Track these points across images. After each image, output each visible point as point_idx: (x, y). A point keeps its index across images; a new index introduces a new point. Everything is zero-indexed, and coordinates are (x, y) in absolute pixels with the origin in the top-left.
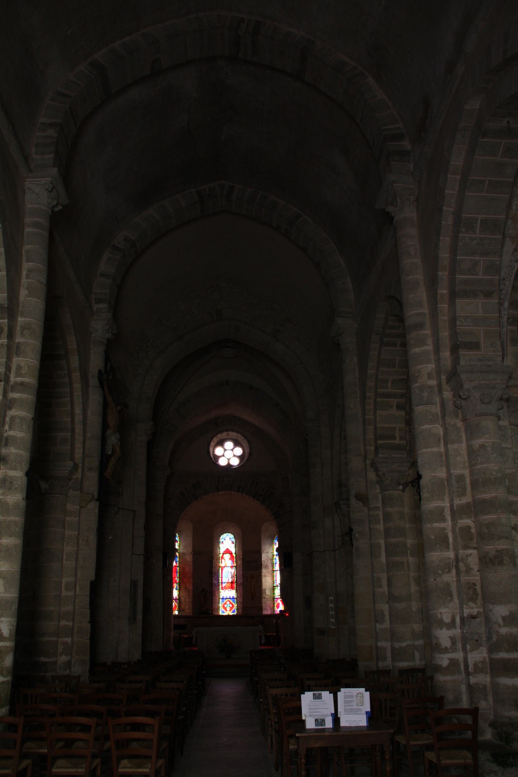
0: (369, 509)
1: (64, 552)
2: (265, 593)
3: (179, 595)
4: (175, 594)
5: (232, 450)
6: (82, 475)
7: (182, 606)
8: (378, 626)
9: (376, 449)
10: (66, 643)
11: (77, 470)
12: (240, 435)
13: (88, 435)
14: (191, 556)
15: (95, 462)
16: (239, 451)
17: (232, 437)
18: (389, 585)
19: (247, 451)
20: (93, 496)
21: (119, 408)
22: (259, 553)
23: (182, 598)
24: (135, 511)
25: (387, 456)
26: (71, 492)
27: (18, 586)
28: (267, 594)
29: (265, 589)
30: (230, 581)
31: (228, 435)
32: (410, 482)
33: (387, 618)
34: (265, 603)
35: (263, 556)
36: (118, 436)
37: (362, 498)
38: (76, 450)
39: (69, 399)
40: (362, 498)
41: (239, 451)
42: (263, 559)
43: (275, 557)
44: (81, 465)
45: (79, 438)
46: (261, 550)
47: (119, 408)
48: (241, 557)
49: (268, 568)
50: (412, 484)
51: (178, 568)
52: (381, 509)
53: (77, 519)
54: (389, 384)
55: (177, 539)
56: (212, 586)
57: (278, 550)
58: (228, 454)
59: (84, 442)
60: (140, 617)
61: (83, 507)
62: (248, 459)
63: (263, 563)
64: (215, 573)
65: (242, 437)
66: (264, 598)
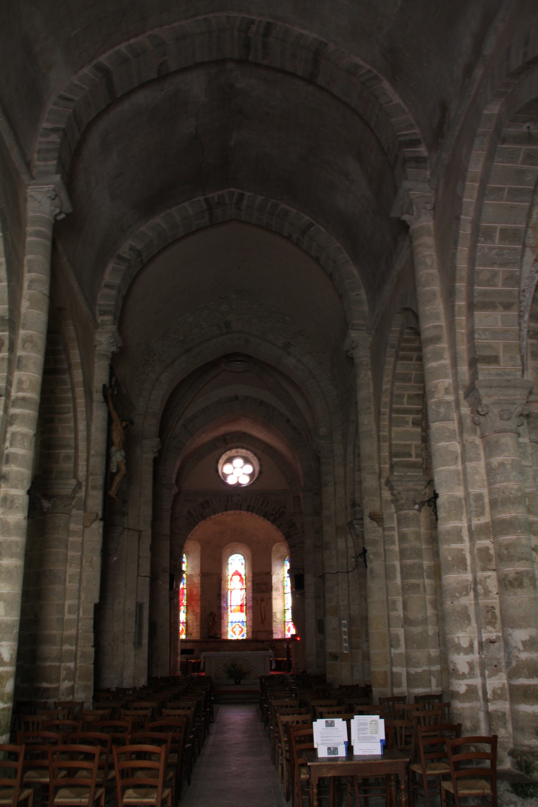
0: (384, 530)
1: (67, 574)
2: (276, 616)
3: (186, 619)
11: (80, 488)
12: (249, 452)
13: (92, 452)
14: (199, 578)
15: (99, 480)
16: (249, 469)
21: (124, 424)
22: (269, 575)
23: (190, 622)
26: (74, 512)
29: (275, 613)
31: (237, 452)
34: (276, 627)
37: (377, 518)
38: (80, 467)
39: (72, 414)
40: (377, 518)
41: (249, 469)
44: (84, 484)
45: (82, 455)
48: (251, 579)
51: (185, 591)
52: (396, 529)
53: (81, 539)
54: (405, 399)
55: (184, 560)
57: (289, 571)
58: (238, 472)
59: (88, 460)
61: (86, 527)
62: (258, 478)
63: (273, 585)
64: (224, 595)
65: (252, 455)
66: (275, 621)
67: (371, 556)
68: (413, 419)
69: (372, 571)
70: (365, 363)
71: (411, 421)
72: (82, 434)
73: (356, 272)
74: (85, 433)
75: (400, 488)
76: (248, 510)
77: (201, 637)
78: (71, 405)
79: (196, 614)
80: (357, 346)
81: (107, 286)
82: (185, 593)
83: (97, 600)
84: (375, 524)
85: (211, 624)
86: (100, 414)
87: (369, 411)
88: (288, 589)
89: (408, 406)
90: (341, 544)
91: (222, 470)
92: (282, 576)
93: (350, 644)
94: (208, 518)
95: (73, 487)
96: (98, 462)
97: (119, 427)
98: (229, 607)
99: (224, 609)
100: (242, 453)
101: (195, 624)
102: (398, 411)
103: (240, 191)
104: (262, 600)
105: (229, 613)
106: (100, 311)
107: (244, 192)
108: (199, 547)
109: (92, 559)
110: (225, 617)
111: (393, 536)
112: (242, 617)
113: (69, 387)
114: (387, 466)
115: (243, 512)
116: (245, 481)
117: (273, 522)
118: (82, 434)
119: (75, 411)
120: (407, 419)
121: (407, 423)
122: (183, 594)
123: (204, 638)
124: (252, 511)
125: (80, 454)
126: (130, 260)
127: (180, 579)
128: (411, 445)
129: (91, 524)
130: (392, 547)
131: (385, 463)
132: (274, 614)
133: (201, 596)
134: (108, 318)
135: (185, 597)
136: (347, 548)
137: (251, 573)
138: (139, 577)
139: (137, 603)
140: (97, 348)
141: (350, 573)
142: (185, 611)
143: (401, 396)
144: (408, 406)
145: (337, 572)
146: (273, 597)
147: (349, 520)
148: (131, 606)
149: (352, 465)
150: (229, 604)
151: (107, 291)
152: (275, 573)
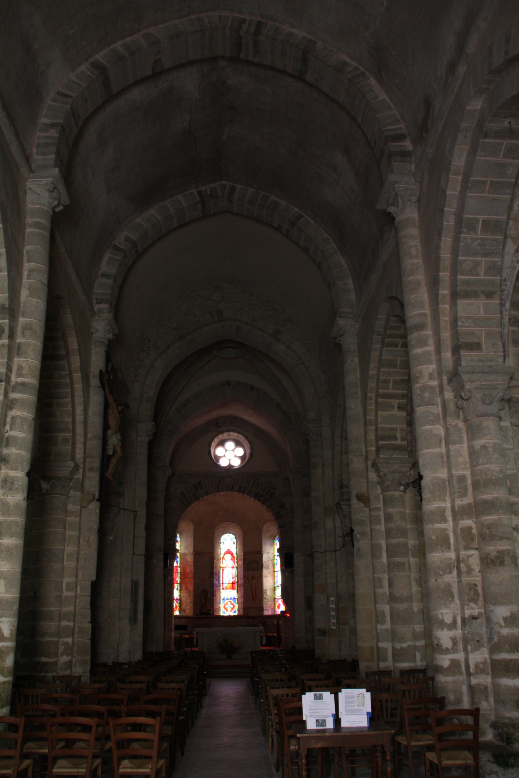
0: (370, 510)
1: (65, 553)
2: (266, 593)
3: (180, 596)
4: (176, 594)
9: (378, 450)
11: (78, 470)
12: (241, 436)
13: (89, 436)
14: (192, 557)
15: (96, 463)
16: (240, 451)
19: (248, 451)
20: (94, 496)
21: (120, 408)
25: (388, 457)
26: (72, 493)
27: (19, 586)
29: (266, 590)
30: (231, 582)
31: (229, 435)
32: (411, 483)
34: (266, 604)
38: (77, 450)
41: (240, 451)
43: (276, 557)
44: (81, 466)
45: (80, 438)
47: (120, 408)
48: (242, 557)
51: (179, 569)
52: (382, 509)
53: (78, 519)
54: (391, 385)
55: (178, 539)
57: (279, 550)
58: (230, 454)
59: (85, 443)
61: (83, 507)
62: (249, 460)
63: (264, 563)
65: (244, 438)
66: (265, 598)
68: (398, 404)
70: (352, 349)
74: (82, 417)
75: (386, 470)
76: (239, 491)
78: (69, 390)
79: (189, 592)
81: (103, 275)
82: (179, 571)
84: (362, 504)
85: (203, 601)
87: (356, 396)
88: (278, 568)
89: (394, 391)
90: (329, 524)
92: (272, 553)
93: (338, 619)
94: (200, 499)
96: (95, 445)
97: (116, 411)
98: (221, 584)
99: (217, 587)
101: (188, 601)
102: (384, 396)
103: (232, 184)
104: (253, 578)
105: (221, 590)
106: (97, 299)
107: (236, 185)
108: (192, 527)
109: (89, 539)
110: (217, 595)
111: (379, 516)
112: (234, 594)
115: (234, 493)
116: (236, 463)
117: (264, 503)
119: (73, 396)
122: (177, 572)
124: (243, 493)
127: (174, 557)
128: (397, 428)
129: (89, 504)
130: (378, 527)
131: (372, 446)
132: (264, 591)
133: (194, 573)
135: (179, 575)
136: (335, 527)
137: (242, 552)
139: (132, 580)
140: (94, 335)
141: (338, 552)
142: (179, 589)
143: (386, 382)
144: (394, 391)
146: (264, 574)
149: (339, 448)
150: (221, 582)
151: (103, 280)
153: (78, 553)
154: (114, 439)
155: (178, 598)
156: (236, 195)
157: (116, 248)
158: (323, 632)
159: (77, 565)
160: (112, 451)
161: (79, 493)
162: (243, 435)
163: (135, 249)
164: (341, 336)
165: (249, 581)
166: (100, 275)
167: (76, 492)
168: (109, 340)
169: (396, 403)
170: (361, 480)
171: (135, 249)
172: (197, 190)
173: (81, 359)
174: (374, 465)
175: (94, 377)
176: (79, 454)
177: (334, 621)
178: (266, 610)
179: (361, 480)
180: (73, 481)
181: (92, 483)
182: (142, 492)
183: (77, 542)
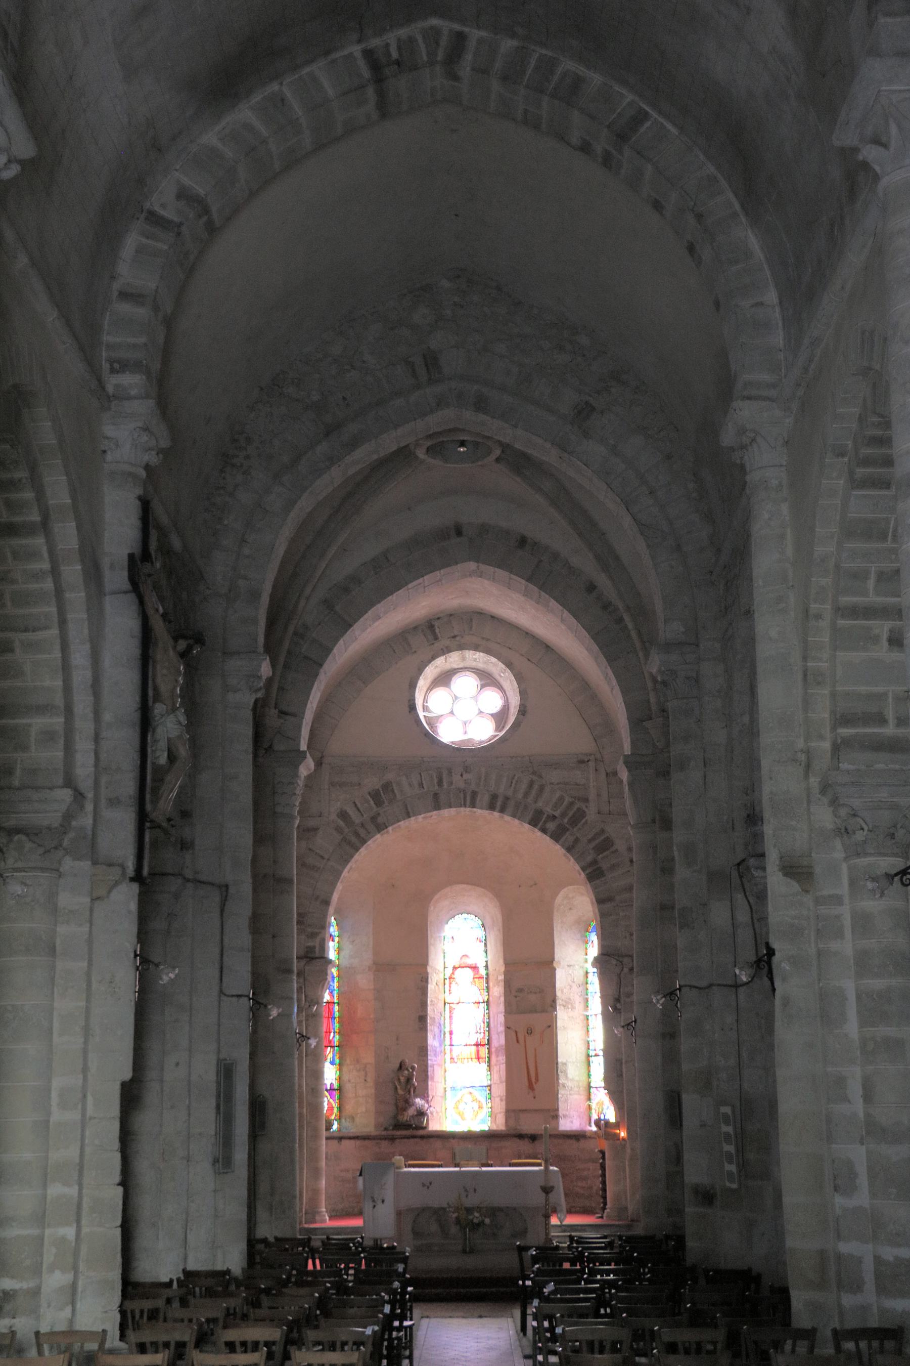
0: (818, 901)
1: (55, 1013)
2: (565, 1072)
3: (340, 1079)
4: (330, 1074)
5: (475, 698)
6: (95, 820)
7: (349, 1108)
8: (839, 1201)
9: (836, 748)
10: (63, 1239)
11: (82, 807)
12: (494, 660)
13: (107, 717)
15: (128, 786)
16: (493, 701)
17: (474, 664)
18: (868, 1097)
19: (515, 702)
20: (123, 867)
21: (182, 645)
22: (547, 965)
23: (348, 1087)
24: (227, 886)
25: (863, 767)
26: (68, 863)
28: (570, 1076)
32: (896, 875)
33: (863, 1180)
34: (566, 1101)
35: (558, 977)
36: (183, 719)
37: (798, 871)
38: (78, 756)
39: (55, 632)
40: (798, 871)
41: (493, 701)
42: (558, 985)
43: (590, 975)
44: (90, 795)
45: (84, 726)
46: (552, 960)
47: (182, 645)
48: (501, 977)
49: (573, 1008)
50: (901, 880)
51: (336, 1008)
53: (86, 929)
54: (871, 583)
55: (333, 930)
56: (426, 1055)
57: (597, 962)
58: (464, 708)
59: (97, 738)
60: (241, 1155)
61: (98, 898)
63: (558, 993)
65: (501, 665)
67: (786, 966)
69: (786, 1002)
70: (775, 482)
71: (885, 636)
72: (81, 676)
73: (754, 242)
74: (89, 674)
75: (856, 803)
76: (492, 807)
77: (377, 1126)
78: (54, 609)
80: (753, 440)
81: (124, 295)
82: (337, 1015)
83: (128, 1075)
84: (795, 886)
85: (400, 1092)
86: (121, 622)
88: (596, 1005)
89: (879, 599)
91: (425, 700)
92: (577, 964)
93: (743, 1166)
94: (390, 828)
95: (64, 807)
96: (121, 741)
97: (171, 653)
98: (448, 1048)
100: (475, 660)
102: (854, 612)
103: (457, 27)
104: (530, 1031)
105: (448, 1065)
106: (111, 362)
107: (466, 30)
111: (838, 917)
112: (479, 1074)
113: (46, 566)
114: (827, 745)
115: (479, 811)
116: (483, 732)
117: (556, 836)
118: (81, 676)
119: (63, 622)
120: (877, 631)
121: (876, 639)
122: (331, 1016)
123: (386, 1129)
124: (502, 811)
125: (78, 723)
126: (181, 224)
127: (322, 978)
128: (885, 694)
129: (109, 892)
130: (834, 946)
131: (821, 737)
134: (132, 381)
135: (337, 1026)
137: (501, 961)
138: (224, 998)
139: (219, 1061)
140: (109, 457)
141: (742, 990)
142: (337, 1061)
143: (860, 576)
144: (879, 599)
145: (710, 986)
146: (560, 1023)
147: (740, 856)
148: (205, 1071)
151: (125, 308)
152: (564, 963)
153: (88, 1010)
154: (170, 725)
155: (336, 1086)
156: (469, 57)
157: (154, 218)
158: (707, 1197)
159: (86, 1042)
160: (166, 754)
161: (86, 865)
162: (499, 658)
163: (205, 218)
164: (743, 447)
165: (518, 1042)
166: (116, 294)
167: (77, 863)
168: (147, 467)
169: (886, 629)
170: (793, 823)
171: (205, 218)
172: (363, 46)
173: (79, 528)
174: (825, 788)
175: (112, 567)
176: (84, 768)
177: (733, 1168)
178: (565, 1116)
179: (793, 823)
180: (72, 835)
181: (118, 835)
182: (241, 834)
183: (84, 986)
